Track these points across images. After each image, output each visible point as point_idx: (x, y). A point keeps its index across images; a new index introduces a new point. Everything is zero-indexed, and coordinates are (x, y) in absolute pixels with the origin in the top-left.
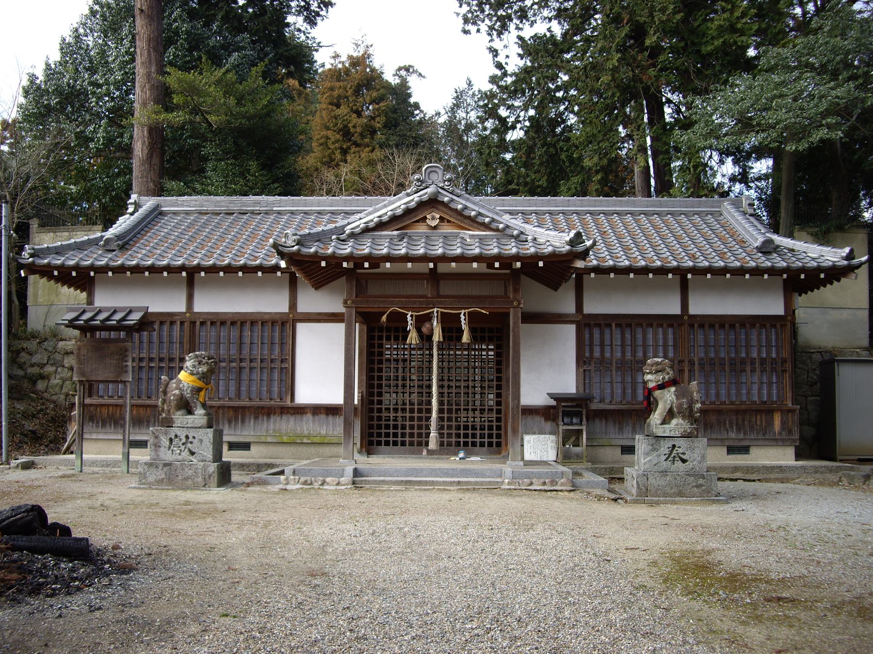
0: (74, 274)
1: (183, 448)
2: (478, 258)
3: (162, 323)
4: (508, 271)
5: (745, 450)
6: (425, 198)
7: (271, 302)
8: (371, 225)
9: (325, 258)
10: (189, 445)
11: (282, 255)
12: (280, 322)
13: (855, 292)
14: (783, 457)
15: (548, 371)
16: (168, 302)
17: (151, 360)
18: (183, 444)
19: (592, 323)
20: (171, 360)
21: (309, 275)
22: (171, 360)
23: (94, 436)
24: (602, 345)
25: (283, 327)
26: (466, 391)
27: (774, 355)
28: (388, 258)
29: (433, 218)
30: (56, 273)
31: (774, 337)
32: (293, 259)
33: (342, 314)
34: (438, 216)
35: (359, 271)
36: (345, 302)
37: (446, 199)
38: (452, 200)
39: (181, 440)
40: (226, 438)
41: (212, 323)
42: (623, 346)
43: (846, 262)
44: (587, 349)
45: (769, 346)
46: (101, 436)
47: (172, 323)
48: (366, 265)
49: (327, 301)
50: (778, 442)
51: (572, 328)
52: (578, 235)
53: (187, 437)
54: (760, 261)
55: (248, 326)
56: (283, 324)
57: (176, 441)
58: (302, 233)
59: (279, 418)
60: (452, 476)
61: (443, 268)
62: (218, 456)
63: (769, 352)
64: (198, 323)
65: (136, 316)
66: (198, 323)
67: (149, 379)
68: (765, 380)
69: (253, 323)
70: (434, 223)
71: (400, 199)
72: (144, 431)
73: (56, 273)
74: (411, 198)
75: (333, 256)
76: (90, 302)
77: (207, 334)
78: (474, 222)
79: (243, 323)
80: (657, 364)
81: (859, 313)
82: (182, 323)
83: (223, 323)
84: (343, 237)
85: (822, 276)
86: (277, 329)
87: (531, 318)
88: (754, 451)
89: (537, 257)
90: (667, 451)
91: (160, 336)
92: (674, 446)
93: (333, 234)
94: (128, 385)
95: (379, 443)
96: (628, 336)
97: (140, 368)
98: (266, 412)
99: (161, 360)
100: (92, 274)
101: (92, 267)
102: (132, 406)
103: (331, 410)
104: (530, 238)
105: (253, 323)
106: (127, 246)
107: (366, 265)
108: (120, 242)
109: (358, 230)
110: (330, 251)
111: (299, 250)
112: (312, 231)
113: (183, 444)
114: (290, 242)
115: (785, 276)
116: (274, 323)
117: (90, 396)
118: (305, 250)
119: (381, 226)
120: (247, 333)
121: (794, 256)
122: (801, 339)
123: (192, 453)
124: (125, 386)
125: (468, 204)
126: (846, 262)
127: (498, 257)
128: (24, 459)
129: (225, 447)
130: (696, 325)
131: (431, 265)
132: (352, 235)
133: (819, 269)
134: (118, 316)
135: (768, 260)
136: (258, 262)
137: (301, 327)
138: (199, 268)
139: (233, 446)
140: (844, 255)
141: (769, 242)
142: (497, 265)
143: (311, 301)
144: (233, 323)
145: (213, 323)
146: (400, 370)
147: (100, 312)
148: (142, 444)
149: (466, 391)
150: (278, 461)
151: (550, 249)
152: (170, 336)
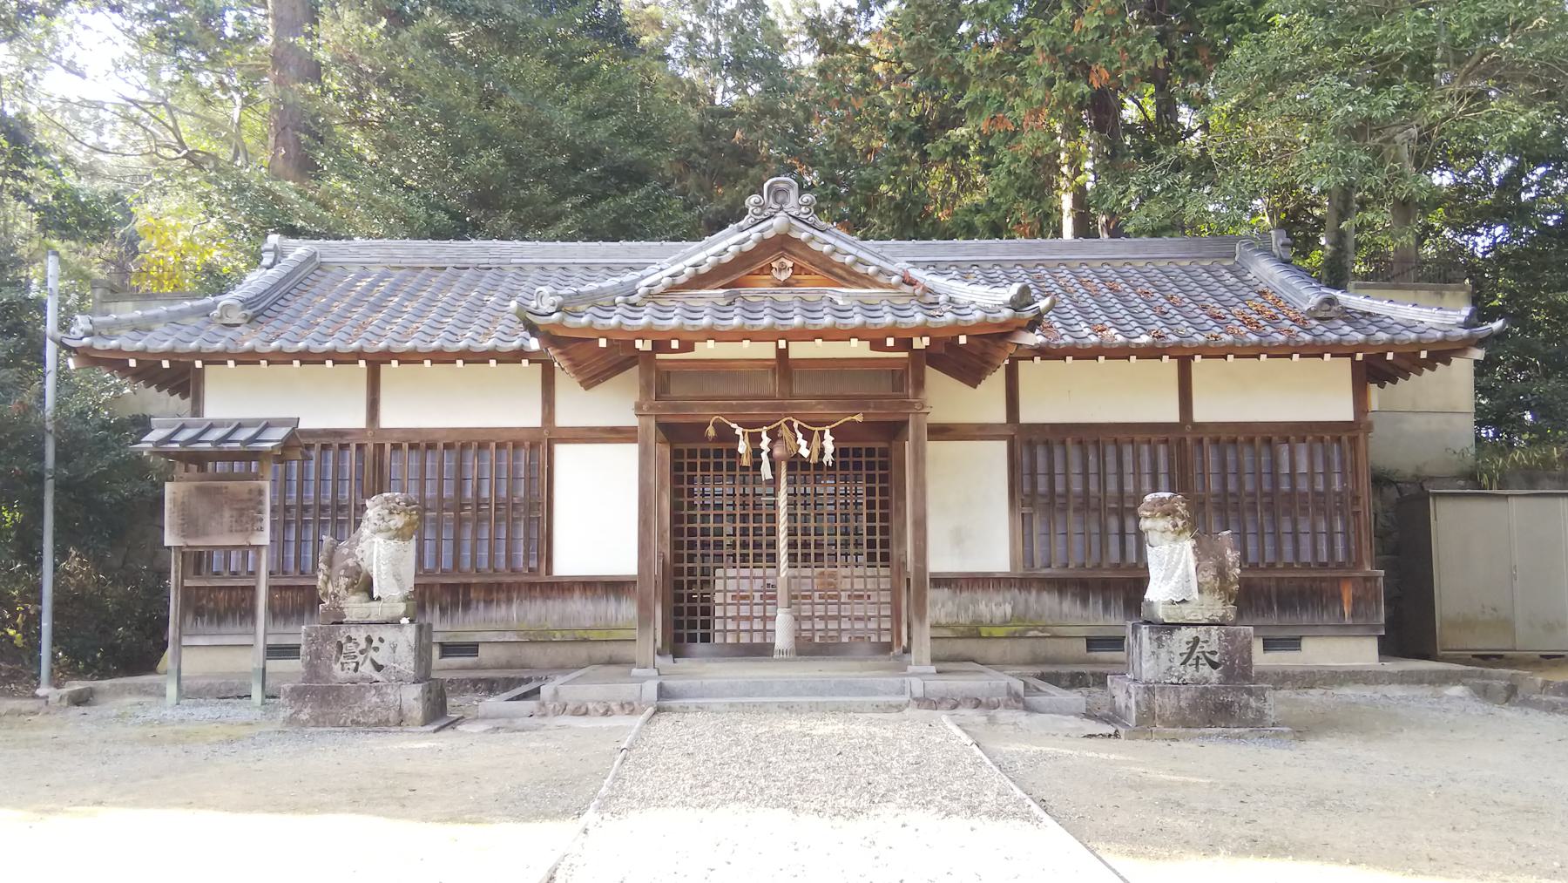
0: (166, 364)
1: (360, 658)
2: (858, 333)
3: (325, 447)
4: (905, 355)
5: (1293, 644)
6: (769, 234)
7: (503, 405)
8: (681, 280)
9: (604, 334)
10: (372, 654)
11: (532, 329)
12: (527, 444)
13: (1455, 384)
14: (1362, 652)
15: (968, 515)
16: (331, 407)
17: (305, 509)
18: (362, 652)
19: (1224, 438)
20: (341, 508)
21: (577, 367)
22: (341, 508)
23: (199, 641)
24: (1051, 475)
25: (533, 452)
26: (731, 551)
27: (1337, 487)
28: (712, 334)
29: (782, 269)
30: (132, 363)
31: (1336, 458)
32: (551, 338)
33: (634, 430)
34: (790, 264)
35: (659, 356)
36: (638, 407)
37: (803, 236)
38: (812, 238)
39: (357, 644)
40: (437, 638)
41: (412, 447)
42: (1085, 474)
43: (1465, 332)
44: (1026, 479)
45: (1327, 475)
46: (217, 641)
47: (343, 447)
48: (675, 344)
49: (615, 404)
50: (1342, 630)
51: (1001, 447)
52: (1025, 290)
53: (369, 640)
54: (1133, 334)
55: (471, 453)
56: (533, 446)
57: (349, 647)
58: (566, 291)
59: (604, 601)
60: (822, 694)
61: (798, 350)
62: (423, 674)
63: (1328, 483)
64: (388, 447)
65: (280, 433)
66: (388, 447)
67: (300, 542)
68: (1322, 526)
69: (482, 446)
70: (784, 276)
71: (726, 237)
72: (292, 628)
73: (132, 363)
74: (746, 234)
75: (619, 329)
76: (197, 410)
77: (400, 465)
78: (848, 276)
79: (464, 447)
80: (1162, 501)
81: (1457, 419)
82: (360, 447)
83: (431, 446)
84: (633, 299)
85: (1424, 355)
86: (523, 453)
87: (941, 432)
88: (1307, 644)
89: (958, 329)
90: (1185, 649)
91: (321, 471)
92: (1196, 640)
93: (618, 294)
94: (264, 553)
95: (692, 639)
96: (1092, 458)
97: (287, 524)
98: (496, 591)
99: (323, 509)
100: (198, 364)
101: (197, 354)
102: (272, 588)
103: (613, 587)
104: (942, 298)
105: (482, 446)
106: (260, 319)
107: (675, 344)
108: (249, 312)
109: (658, 289)
110: (613, 322)
111: (562, 320)
112: (582, 289)
113: (362, 652)
114: (546, 307)
115: (1359, 356)
116: (517, 445)
117: (198, 572)
118: (571, 321)
119: (698, 281)
120: (471, 461)
121: (1372, 323)
122: (1371, 458)
123: (379, 668)
124: (258, 554)
125: (839, 244)
126: (1465, 332)
127: (891, 331)
128: (77, 685)
129: (436, 652)
130: (1206, 440)
131: (782, 344)
132: (650, 296)
133: (1419, 344)
134: (216, 434)
135: (1330, 330)
136: (382, 345)
137: (563, 452)
138: (387, 356)
139: (448, 649)
140: (1462, 319)
141: (1331, 301)
142: (890, 342)
143: (579, 406)
144: (447, 446)
145: (412, 447)
146: (852, 517)
147: (211, 427)
148: (290, 651)
149: (731, 551)
150: (533, 674)
151: (978, 315)
152: (338, 469)
